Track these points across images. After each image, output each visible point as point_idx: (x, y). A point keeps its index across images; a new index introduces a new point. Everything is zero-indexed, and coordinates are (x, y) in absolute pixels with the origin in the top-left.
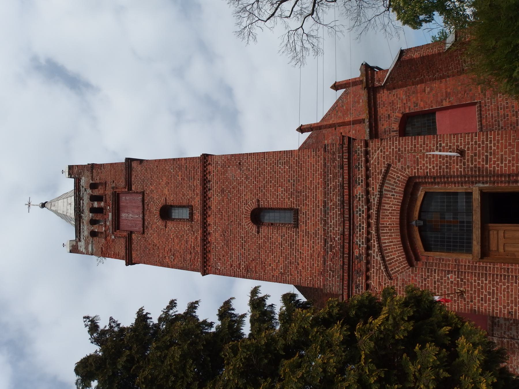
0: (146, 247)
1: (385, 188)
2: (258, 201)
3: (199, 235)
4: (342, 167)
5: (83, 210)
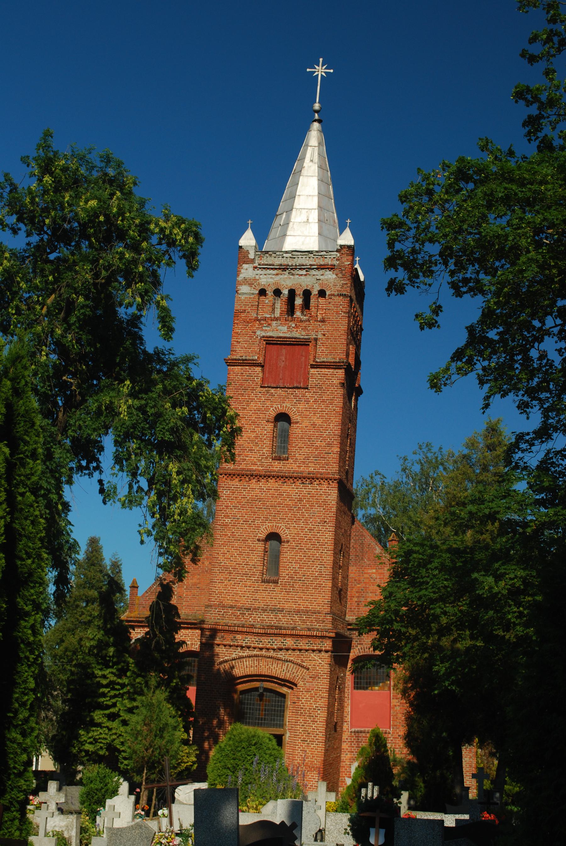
0: (245, 389)
1: (290, 664)
2: (288, 542)
3: (257, 468)
4: (309, 629)
5: (293, 275)
